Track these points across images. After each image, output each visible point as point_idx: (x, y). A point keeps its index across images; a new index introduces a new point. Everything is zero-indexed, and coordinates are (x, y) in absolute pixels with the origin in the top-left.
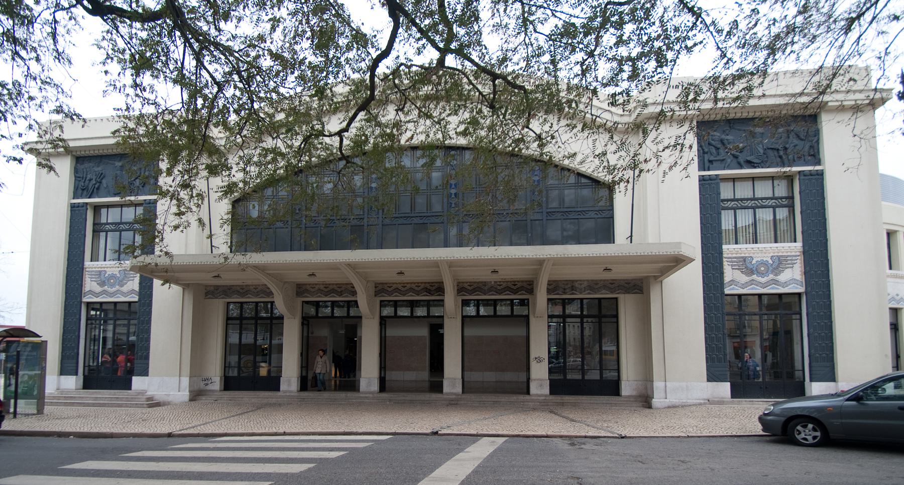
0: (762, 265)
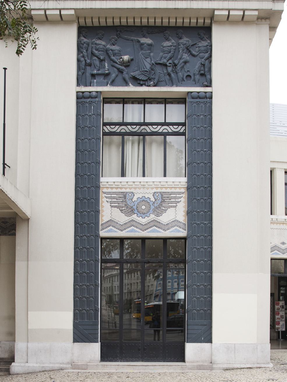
0: (143, 203)
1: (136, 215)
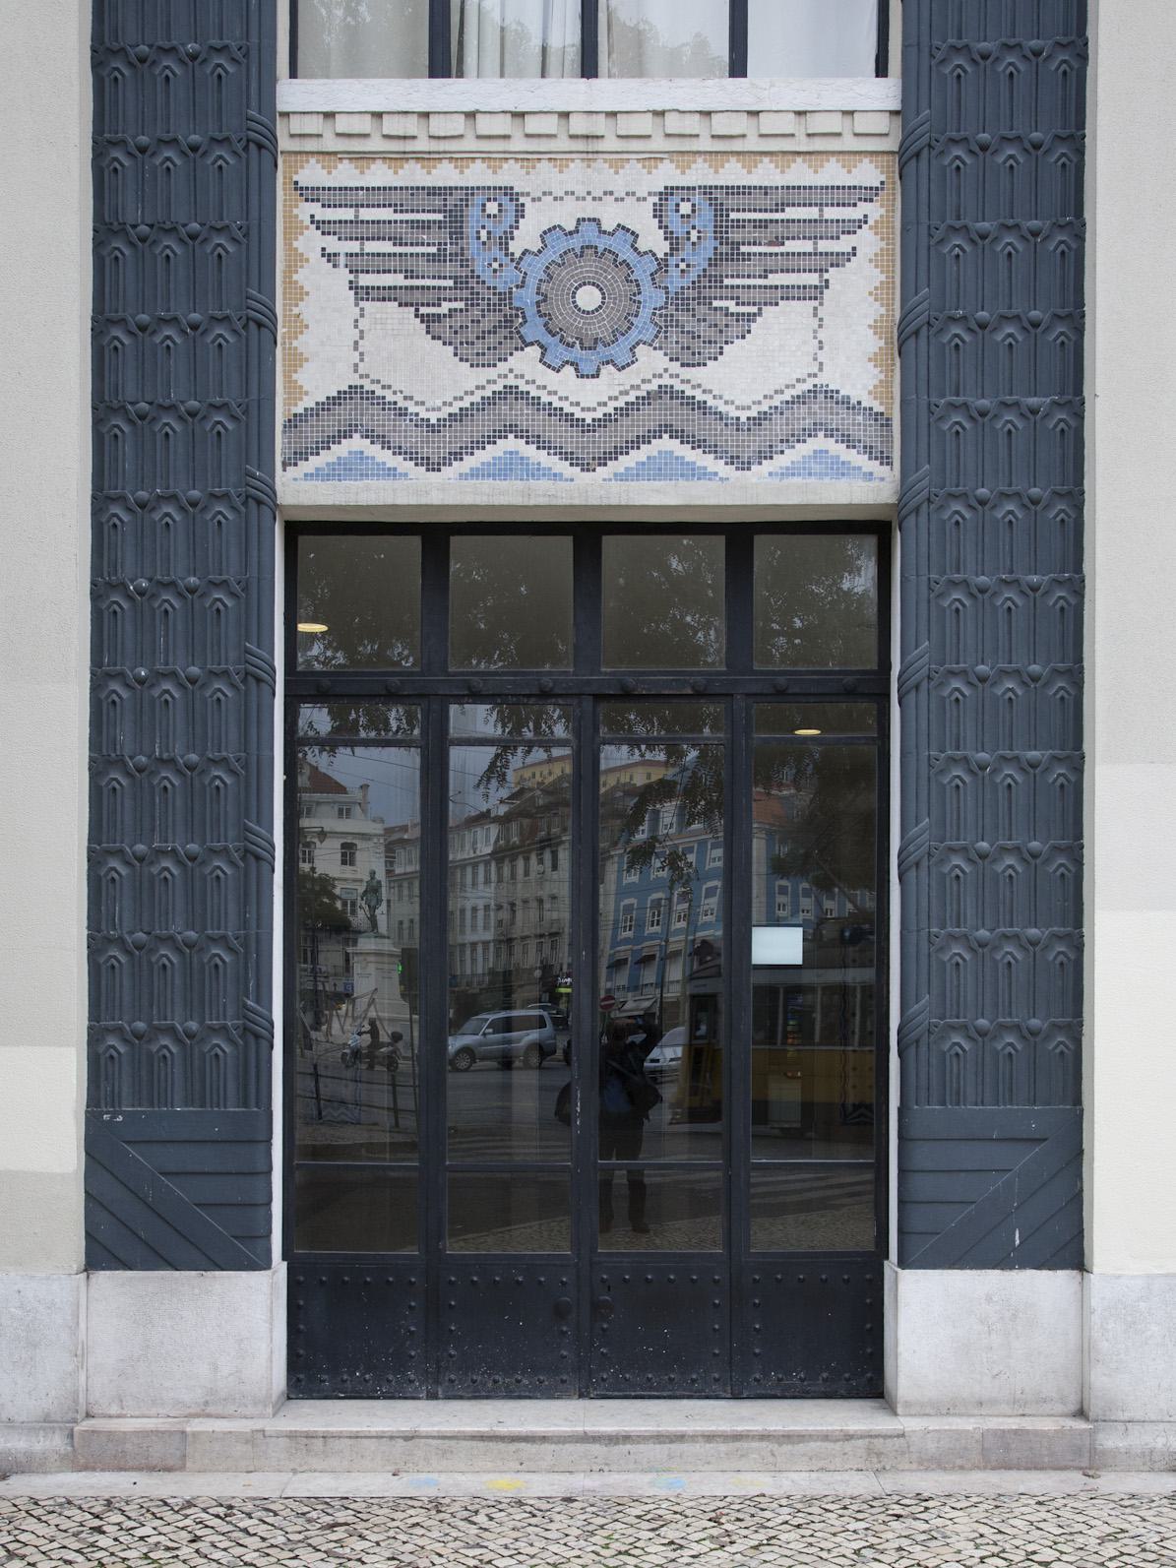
0: (588, 266)
1: (534, 352)
